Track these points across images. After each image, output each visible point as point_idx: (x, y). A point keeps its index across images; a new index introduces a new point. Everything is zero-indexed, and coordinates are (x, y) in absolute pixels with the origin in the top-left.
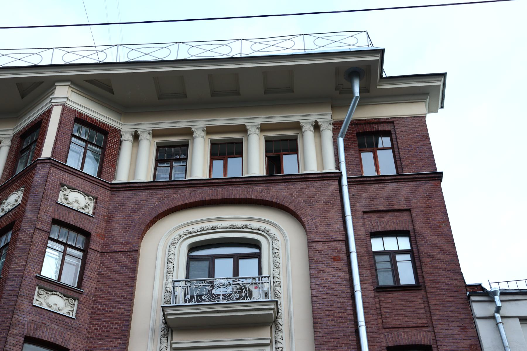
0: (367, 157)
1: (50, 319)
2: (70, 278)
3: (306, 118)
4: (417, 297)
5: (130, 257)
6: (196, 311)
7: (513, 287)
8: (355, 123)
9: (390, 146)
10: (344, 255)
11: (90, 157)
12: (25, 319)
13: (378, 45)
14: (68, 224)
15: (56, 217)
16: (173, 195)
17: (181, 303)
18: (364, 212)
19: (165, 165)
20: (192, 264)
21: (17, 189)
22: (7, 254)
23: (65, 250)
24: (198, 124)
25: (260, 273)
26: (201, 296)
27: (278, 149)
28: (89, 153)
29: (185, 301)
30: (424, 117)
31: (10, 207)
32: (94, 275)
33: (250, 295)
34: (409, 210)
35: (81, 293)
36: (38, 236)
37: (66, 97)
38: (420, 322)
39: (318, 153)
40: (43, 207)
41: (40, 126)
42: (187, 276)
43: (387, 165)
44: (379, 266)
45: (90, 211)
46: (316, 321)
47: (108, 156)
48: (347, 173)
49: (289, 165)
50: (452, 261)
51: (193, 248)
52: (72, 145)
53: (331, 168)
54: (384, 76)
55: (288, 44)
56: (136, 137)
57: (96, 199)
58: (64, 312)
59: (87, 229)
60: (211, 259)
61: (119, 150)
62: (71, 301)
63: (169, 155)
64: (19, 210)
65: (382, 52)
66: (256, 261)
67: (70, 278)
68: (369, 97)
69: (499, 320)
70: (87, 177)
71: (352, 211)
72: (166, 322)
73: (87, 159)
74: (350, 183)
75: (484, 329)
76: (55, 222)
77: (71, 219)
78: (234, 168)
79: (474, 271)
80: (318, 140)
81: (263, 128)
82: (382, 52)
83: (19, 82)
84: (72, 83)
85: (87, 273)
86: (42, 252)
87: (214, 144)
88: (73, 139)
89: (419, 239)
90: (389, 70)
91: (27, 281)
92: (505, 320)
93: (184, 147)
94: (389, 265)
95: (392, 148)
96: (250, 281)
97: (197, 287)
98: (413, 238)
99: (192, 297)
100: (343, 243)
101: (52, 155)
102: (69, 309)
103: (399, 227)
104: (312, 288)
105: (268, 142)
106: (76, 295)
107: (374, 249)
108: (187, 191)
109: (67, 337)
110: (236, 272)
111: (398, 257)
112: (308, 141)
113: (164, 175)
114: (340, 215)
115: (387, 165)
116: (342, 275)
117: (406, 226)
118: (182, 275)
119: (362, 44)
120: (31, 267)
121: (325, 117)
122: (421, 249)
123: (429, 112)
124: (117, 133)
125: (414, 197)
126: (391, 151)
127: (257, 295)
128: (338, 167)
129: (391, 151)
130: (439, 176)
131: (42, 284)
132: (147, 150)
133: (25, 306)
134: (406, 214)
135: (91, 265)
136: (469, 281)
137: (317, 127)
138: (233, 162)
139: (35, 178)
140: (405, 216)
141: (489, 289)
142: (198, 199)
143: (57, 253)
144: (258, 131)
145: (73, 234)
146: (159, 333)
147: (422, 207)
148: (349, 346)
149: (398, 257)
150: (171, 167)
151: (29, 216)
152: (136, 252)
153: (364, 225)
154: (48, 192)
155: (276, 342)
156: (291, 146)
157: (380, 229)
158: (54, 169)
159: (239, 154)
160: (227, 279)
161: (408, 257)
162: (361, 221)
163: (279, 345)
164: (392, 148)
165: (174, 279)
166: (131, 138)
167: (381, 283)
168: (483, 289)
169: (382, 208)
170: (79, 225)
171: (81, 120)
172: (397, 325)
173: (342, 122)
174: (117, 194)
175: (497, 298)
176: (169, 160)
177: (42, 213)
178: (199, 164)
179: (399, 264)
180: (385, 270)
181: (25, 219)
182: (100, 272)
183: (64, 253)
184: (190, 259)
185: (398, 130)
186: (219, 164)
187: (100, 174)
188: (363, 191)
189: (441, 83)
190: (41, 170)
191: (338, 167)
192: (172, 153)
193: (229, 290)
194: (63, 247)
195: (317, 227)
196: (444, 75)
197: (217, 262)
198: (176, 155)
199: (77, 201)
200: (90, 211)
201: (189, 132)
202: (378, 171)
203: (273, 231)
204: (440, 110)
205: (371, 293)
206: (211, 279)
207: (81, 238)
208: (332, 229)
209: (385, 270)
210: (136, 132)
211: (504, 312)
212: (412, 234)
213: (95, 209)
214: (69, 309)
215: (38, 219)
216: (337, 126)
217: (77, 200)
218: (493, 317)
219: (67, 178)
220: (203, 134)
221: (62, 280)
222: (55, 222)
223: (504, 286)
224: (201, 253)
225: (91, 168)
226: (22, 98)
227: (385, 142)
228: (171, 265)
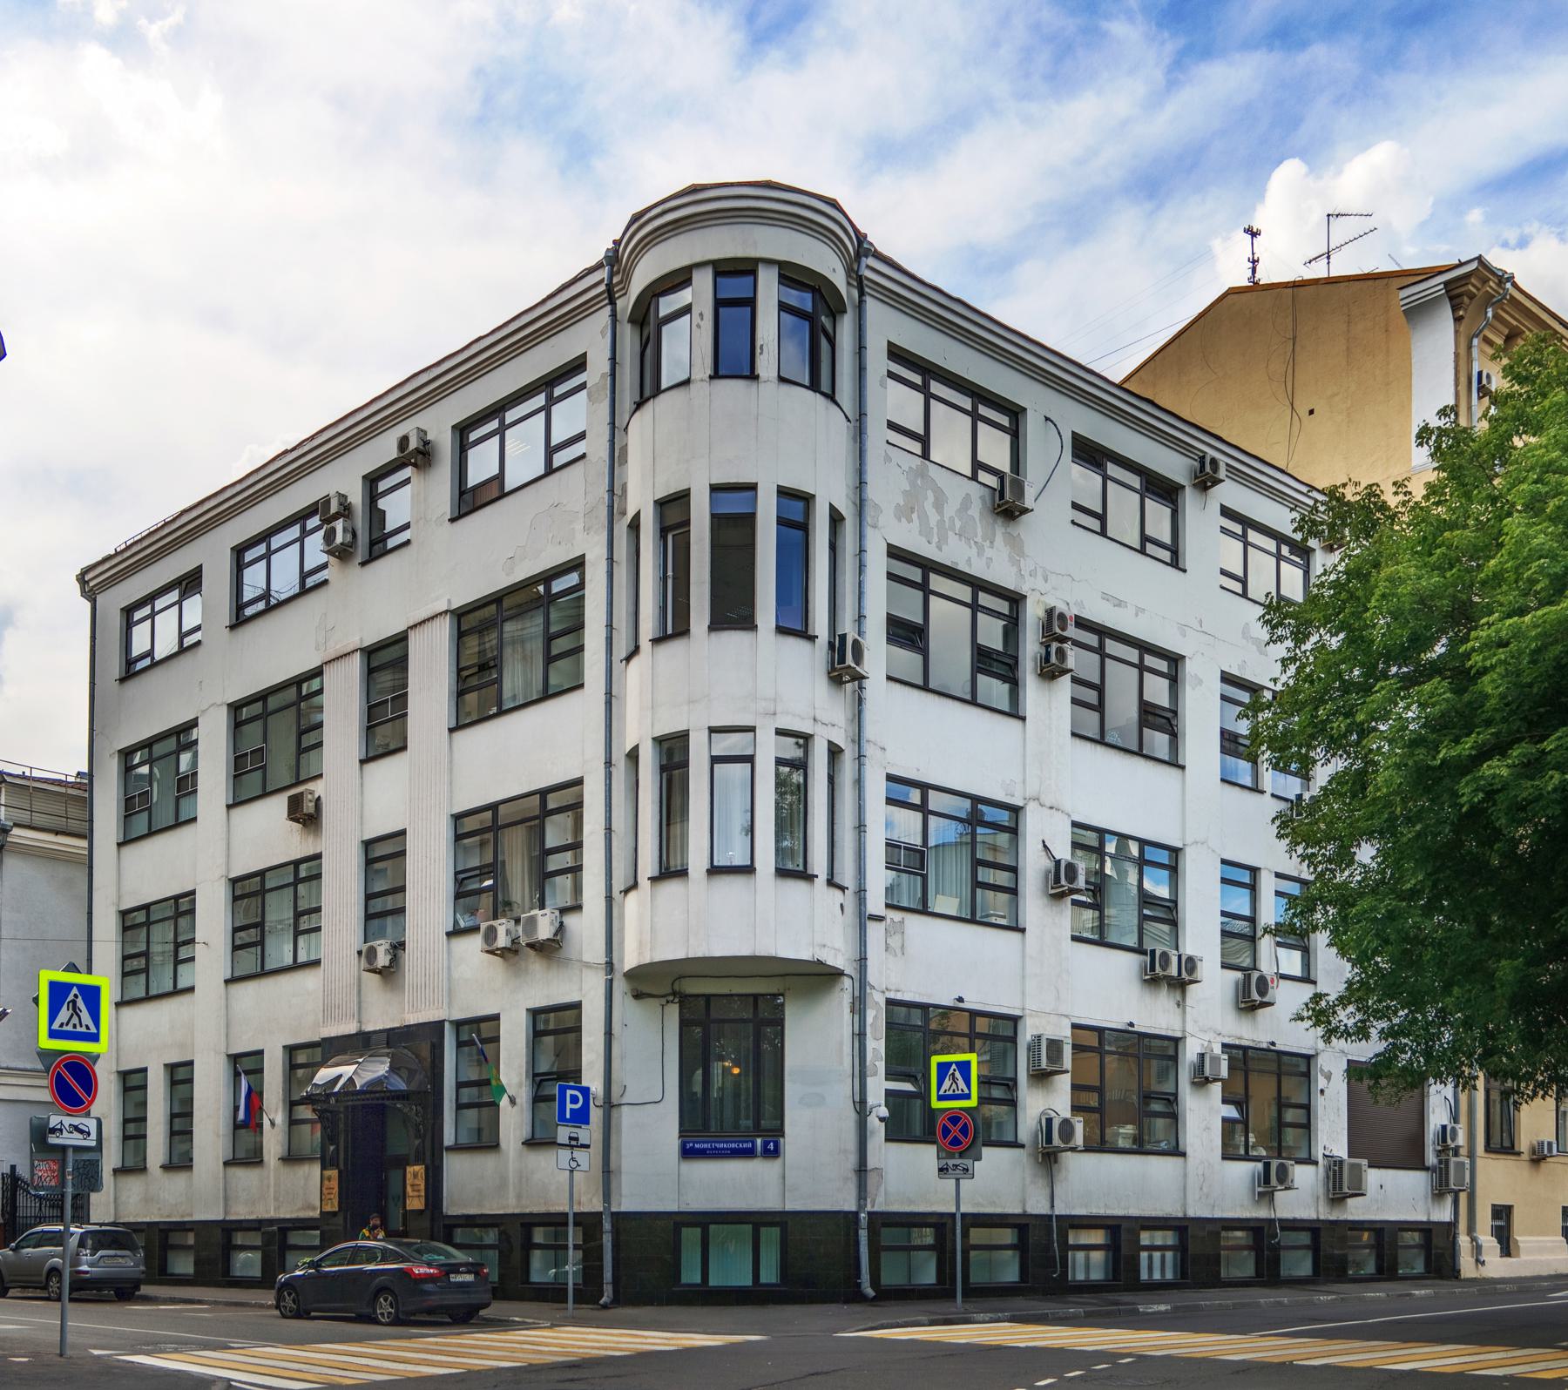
180: (1152, 1238)
202: (607, 1197)
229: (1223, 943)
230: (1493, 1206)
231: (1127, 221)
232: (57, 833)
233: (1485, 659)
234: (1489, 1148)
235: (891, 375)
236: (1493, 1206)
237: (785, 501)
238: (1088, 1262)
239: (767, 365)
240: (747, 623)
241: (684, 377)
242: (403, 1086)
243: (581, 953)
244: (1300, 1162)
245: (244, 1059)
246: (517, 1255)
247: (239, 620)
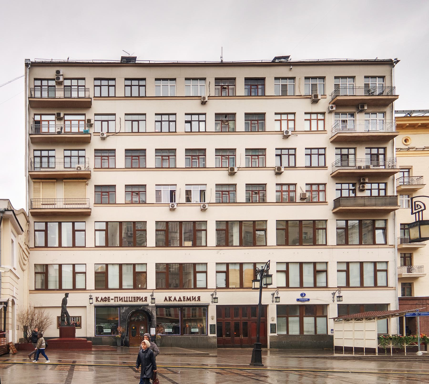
9: (372, 195)
15: (186, 120)
19: (139, 62)
79: (394, 138)
86: (193, 310)
160: (349, 372)
183: (102, 195)
229: (29, 191)
232: (392, 76)
234: (277, 305)
237: (401, 301)
239: (236, 240)
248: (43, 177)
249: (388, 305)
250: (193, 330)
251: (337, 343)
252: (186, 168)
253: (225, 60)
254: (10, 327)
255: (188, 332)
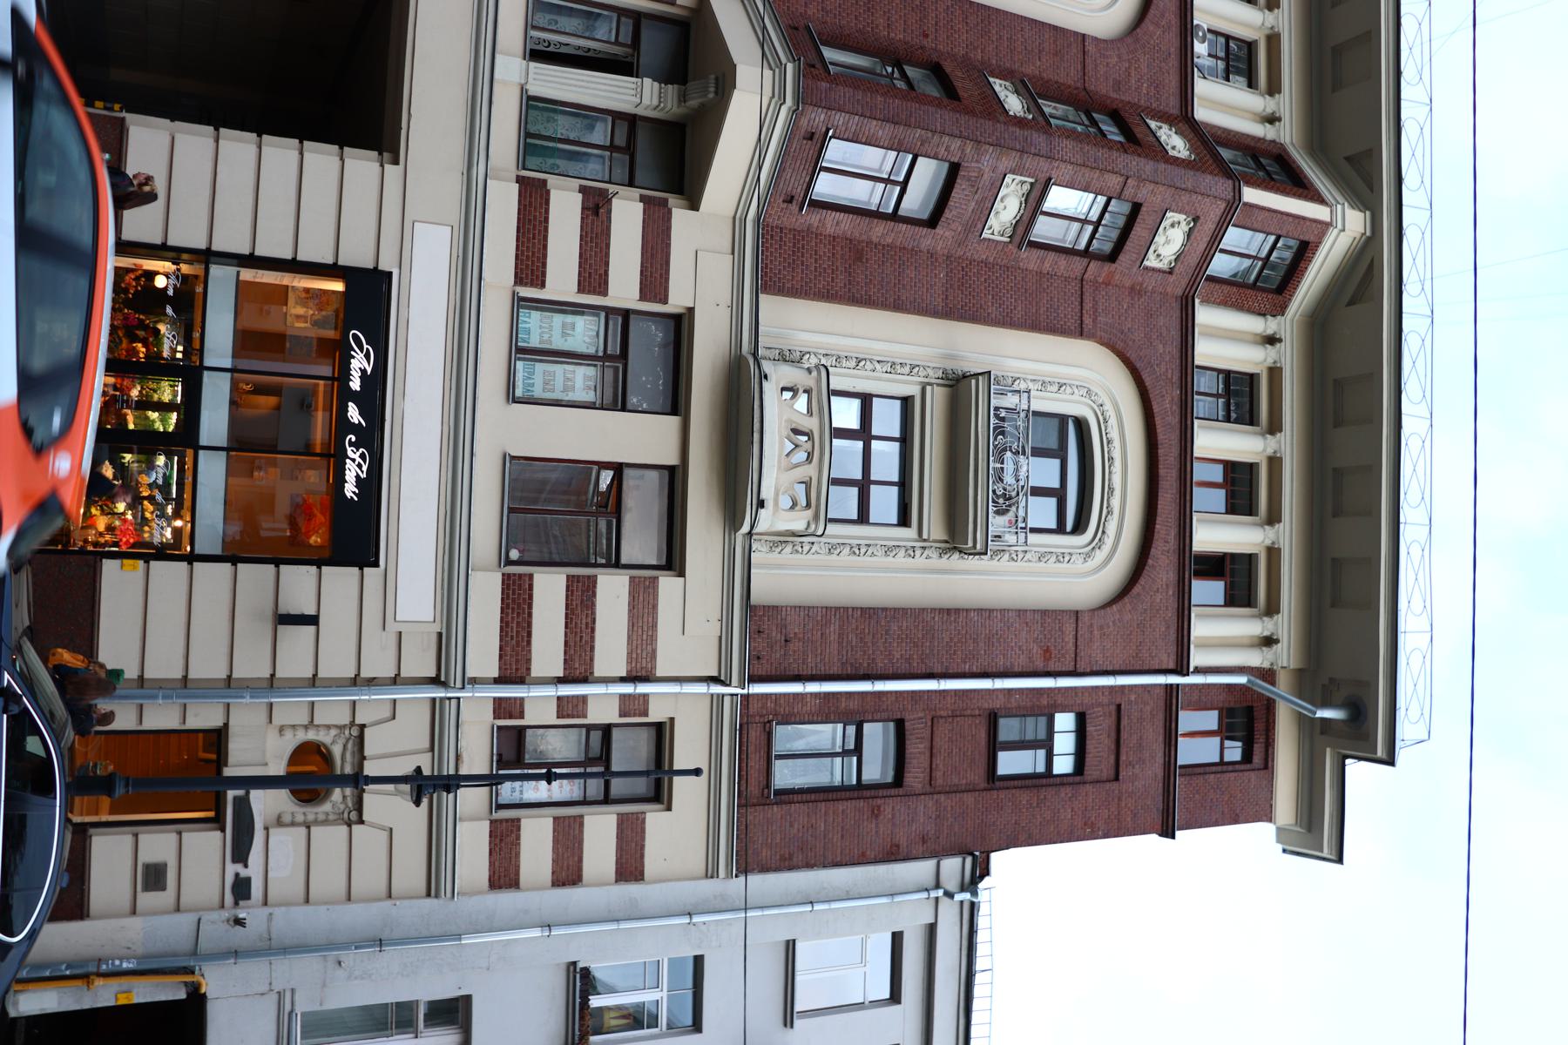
0: (1210, 720)
1: (984, 199)
2: (1044, 229)
3: (1286, 624)
4: (977, 776)
5: (1072, 323)
6: (980, 424)
7: (982, 922)
8: (1270, 706)
10: (1052, 667)
11: (1240, 264)
12: (986, 162)
13: (1401, 755)
14: (1133, 225)
16: (1170, 394)
17: (994, 403)
18: (1119, 706)
20: (1056, 422)
21: (1192, 149)
22: (1088, 135)
23: (1089, 222)
24: (1288, 444)
25: (1033, 530)
26: (1003, 433)
27: (1238, 578)
28: (1247, 263)
29: (997, 409)
30: (1270, 820)
31: (1163, 138)
32: (1047, 266)
33: (999, 513)
34: (1117, 779)
35: (1020, 247)
36: (1114, 181)
37: (1345, 227)
38: (938, 774)
39: (1223, 640)
40: (1161, 188)
41: (1297, 185)
42: (1036, 413)
43: (1193, 751)
44: (1030, 721)
45: (1151, 261)
46: (950, 613)
47: (1237, 293)
48: (1185, 686)
49: (1207, 591)
50: (1030, 836)
51: (1081, 425)
52: (1261, 236)
53: (1197, 658)
54: (1348, 761)
55: (1417, 605)
56: (1271, 340)
57: (1171, 272)
58: (992, 221)
59: (1121, 257)
60: (1061, 453)
61: (1250, 311)
62: (1009, 232)
63: (1237, 393)
64: (1158, 152)
65: (1390, 761)
66: (1053, 525)
67: (1044, 229)
68: (1313, 734)
69: (933, 894)
70: (1207, 258)
71: (1123, 687)
72: (966, 377)
73: (1237, 259)
74: (1169, 687)
75: (922, 869)
76: (1136, 208)
77: (1139, 231)
78: (1207, 499)
80: (1246, 641)
81: (1273, 552)
82: (1390, 761)
83: (1373, 153)
84: (1369, 239)
85: (1052, 255)
87: (1251, 468)
88: (1272, 238)
89: (1069, 789)
90: (1357, 771)
91: (1043, 164)
92: (932, 902)
93: (1247, 417)
94: (1030, 736)
95: (1222, 763)
96: (1021, 513)
97: (1017, 428)
98: (1071, 779)
99: (1003, 419)
100: (1071, 668)
101: (1246, 204)
102: (997, 228)
103: (1089, 759)
104: (1003, 611)
105: (1250, 559)
106: (1017, 239)
107: (1057, 716)
108: (1174, 420)
109: (953, 226)
110: (1038, 492)
111: (1041, 753)
112: (1245, 626)
113: (1203, 382)
114: (1117, 668)
115: (1193, 751)
116: (1020, 663)
117: (1091, 771)
118: (1037, 406)
119: (1406, 729)
120: (1066, 171)
121: (1285, 656)
122: (1052, 791)
123: (1278, 829)
124: (1280, 310)
125: (1139, 786)
126: (1217, 760)
127: (998, 523)
128: (1198, 671)
129: (1217, 760)
130: (1171, 835)
131: (1039, 187)
132: (1248, 358)
133: (1006, 162)
134: (1112, 773)
135: (1063, 261)
136: (996, 858)
137: (1268, 641)
138: (1220, 496)
139: (1209, 177)
140: (1106, 769)
141: (981, 886)
142: (1160, 437)
143: (1085, 210)
144: (1268, 542)
145: (1115, 235)
146: (949, 365)
147: (1120, 799)
148: (909, 660)
149: (1041, 753)
150: (1217, 396)
151: (1148, 166)
152: (1081, 333)
153: (1100, 704)
154: (1185, 197)
155: (924, 548)
156: (1239, 597)
157: (1090, 728)
158: (1224, 205)
159: (1231, 509)
161: (1041, 768)
162: (1106, 701)
163: (918, 552)
164: (1222, 763)
165: (1033, 393)
166: (1270, 332)
167: (1002, 722)
168: (982, 877)
169: (1124, 735)
170: (1129, 245)
171: (1304, 252)
172: (937, 739)
173: (1273, 683)
174: (1176, 306)
175: (967, 896)
176: (1228, 393)
177: (1152, 186)
178: (1217, 442)
179: (1031, 752)
180: (1023, 730)
181: (1142, 161)
182: (1050, 275)
183: (1085, 222)
184: (1063, 419)
185: (1252, 774)
186: (1217, 474)
187: (1211, 279)
188: (1156, 706)
189: (1325, 854)
190: (1223, 187)
191: (1198, 671)
192: (1241, 398)
193: (1009, 478)
194: (1095, 219)
195: (1101, 628)
196: (1340, 860)
197: (1057, 462)
198: (1237, 405)
199: (1168, 242)
200: (1151, 261)
201: (1274, 427)
202: (1184, 735)
203: (1100, 556)
204: (1280, 847)
205: (988, 705)
206: (1029, 451)
207: (1108, 248)
208: (1095, 653)
209: (1023, 730)
210: (1280, 340)
211: (945, 903)
212: (1078, 779)
213: (1153, 269)
214: (997, 228)
215: (1141, 180)
216: (1268, 675)
217: (1170, 242)
218: (937, 886)
219: (1208, 226)
220: (1270, 451)
221: (1041, 218)
222: (1136, 208)
223: (983, 910)
224: (1072, 438)
225: (1221, 265)
226: (1347, 159)
227: (1234, 752)
228: (1055, 388)
230: (467, 999)
231: (437, 628)
233: (555, 537)
235: (897, 938)
236: (467, 999)
238: (392, 1017)
240: (497, 716)
241: (385, 834)
242: (150, 413)
243: (661, 478)
244: (221, 759)
245: (84, 283)
246: (756, 763)
247: (349, 978)
248: (30, 986)
249: (694, 205)
250: (603, 486)
251: (101, 659)
252: (157, 273)
253: (260, 251)
254: (963, 119)
255: (817, 118)
